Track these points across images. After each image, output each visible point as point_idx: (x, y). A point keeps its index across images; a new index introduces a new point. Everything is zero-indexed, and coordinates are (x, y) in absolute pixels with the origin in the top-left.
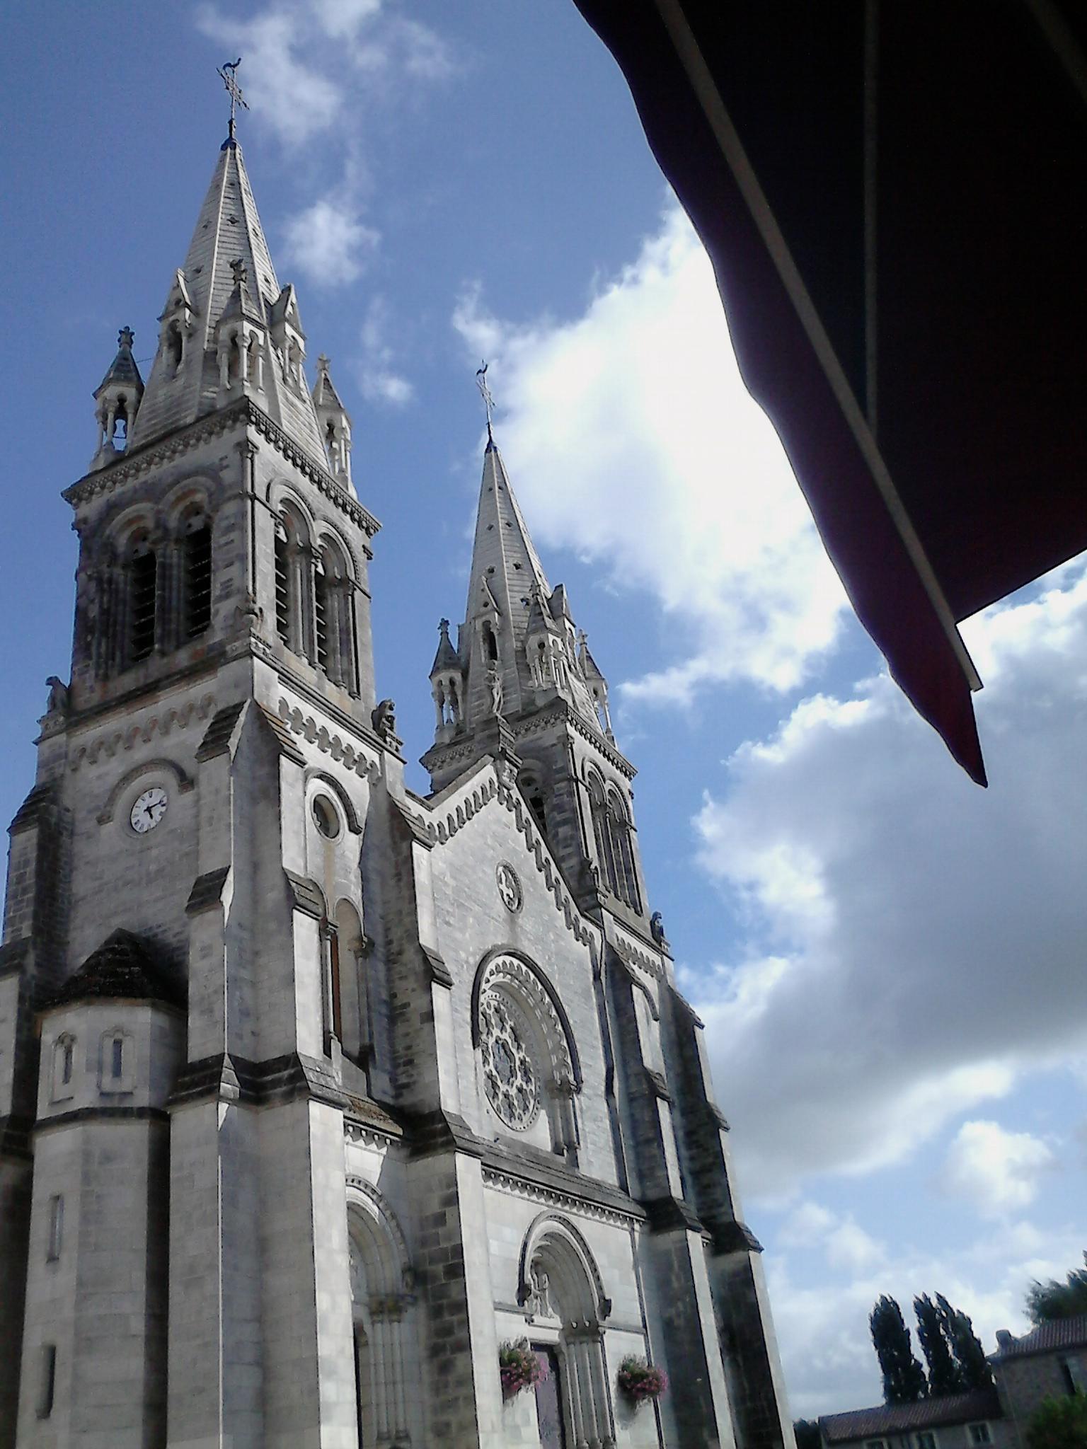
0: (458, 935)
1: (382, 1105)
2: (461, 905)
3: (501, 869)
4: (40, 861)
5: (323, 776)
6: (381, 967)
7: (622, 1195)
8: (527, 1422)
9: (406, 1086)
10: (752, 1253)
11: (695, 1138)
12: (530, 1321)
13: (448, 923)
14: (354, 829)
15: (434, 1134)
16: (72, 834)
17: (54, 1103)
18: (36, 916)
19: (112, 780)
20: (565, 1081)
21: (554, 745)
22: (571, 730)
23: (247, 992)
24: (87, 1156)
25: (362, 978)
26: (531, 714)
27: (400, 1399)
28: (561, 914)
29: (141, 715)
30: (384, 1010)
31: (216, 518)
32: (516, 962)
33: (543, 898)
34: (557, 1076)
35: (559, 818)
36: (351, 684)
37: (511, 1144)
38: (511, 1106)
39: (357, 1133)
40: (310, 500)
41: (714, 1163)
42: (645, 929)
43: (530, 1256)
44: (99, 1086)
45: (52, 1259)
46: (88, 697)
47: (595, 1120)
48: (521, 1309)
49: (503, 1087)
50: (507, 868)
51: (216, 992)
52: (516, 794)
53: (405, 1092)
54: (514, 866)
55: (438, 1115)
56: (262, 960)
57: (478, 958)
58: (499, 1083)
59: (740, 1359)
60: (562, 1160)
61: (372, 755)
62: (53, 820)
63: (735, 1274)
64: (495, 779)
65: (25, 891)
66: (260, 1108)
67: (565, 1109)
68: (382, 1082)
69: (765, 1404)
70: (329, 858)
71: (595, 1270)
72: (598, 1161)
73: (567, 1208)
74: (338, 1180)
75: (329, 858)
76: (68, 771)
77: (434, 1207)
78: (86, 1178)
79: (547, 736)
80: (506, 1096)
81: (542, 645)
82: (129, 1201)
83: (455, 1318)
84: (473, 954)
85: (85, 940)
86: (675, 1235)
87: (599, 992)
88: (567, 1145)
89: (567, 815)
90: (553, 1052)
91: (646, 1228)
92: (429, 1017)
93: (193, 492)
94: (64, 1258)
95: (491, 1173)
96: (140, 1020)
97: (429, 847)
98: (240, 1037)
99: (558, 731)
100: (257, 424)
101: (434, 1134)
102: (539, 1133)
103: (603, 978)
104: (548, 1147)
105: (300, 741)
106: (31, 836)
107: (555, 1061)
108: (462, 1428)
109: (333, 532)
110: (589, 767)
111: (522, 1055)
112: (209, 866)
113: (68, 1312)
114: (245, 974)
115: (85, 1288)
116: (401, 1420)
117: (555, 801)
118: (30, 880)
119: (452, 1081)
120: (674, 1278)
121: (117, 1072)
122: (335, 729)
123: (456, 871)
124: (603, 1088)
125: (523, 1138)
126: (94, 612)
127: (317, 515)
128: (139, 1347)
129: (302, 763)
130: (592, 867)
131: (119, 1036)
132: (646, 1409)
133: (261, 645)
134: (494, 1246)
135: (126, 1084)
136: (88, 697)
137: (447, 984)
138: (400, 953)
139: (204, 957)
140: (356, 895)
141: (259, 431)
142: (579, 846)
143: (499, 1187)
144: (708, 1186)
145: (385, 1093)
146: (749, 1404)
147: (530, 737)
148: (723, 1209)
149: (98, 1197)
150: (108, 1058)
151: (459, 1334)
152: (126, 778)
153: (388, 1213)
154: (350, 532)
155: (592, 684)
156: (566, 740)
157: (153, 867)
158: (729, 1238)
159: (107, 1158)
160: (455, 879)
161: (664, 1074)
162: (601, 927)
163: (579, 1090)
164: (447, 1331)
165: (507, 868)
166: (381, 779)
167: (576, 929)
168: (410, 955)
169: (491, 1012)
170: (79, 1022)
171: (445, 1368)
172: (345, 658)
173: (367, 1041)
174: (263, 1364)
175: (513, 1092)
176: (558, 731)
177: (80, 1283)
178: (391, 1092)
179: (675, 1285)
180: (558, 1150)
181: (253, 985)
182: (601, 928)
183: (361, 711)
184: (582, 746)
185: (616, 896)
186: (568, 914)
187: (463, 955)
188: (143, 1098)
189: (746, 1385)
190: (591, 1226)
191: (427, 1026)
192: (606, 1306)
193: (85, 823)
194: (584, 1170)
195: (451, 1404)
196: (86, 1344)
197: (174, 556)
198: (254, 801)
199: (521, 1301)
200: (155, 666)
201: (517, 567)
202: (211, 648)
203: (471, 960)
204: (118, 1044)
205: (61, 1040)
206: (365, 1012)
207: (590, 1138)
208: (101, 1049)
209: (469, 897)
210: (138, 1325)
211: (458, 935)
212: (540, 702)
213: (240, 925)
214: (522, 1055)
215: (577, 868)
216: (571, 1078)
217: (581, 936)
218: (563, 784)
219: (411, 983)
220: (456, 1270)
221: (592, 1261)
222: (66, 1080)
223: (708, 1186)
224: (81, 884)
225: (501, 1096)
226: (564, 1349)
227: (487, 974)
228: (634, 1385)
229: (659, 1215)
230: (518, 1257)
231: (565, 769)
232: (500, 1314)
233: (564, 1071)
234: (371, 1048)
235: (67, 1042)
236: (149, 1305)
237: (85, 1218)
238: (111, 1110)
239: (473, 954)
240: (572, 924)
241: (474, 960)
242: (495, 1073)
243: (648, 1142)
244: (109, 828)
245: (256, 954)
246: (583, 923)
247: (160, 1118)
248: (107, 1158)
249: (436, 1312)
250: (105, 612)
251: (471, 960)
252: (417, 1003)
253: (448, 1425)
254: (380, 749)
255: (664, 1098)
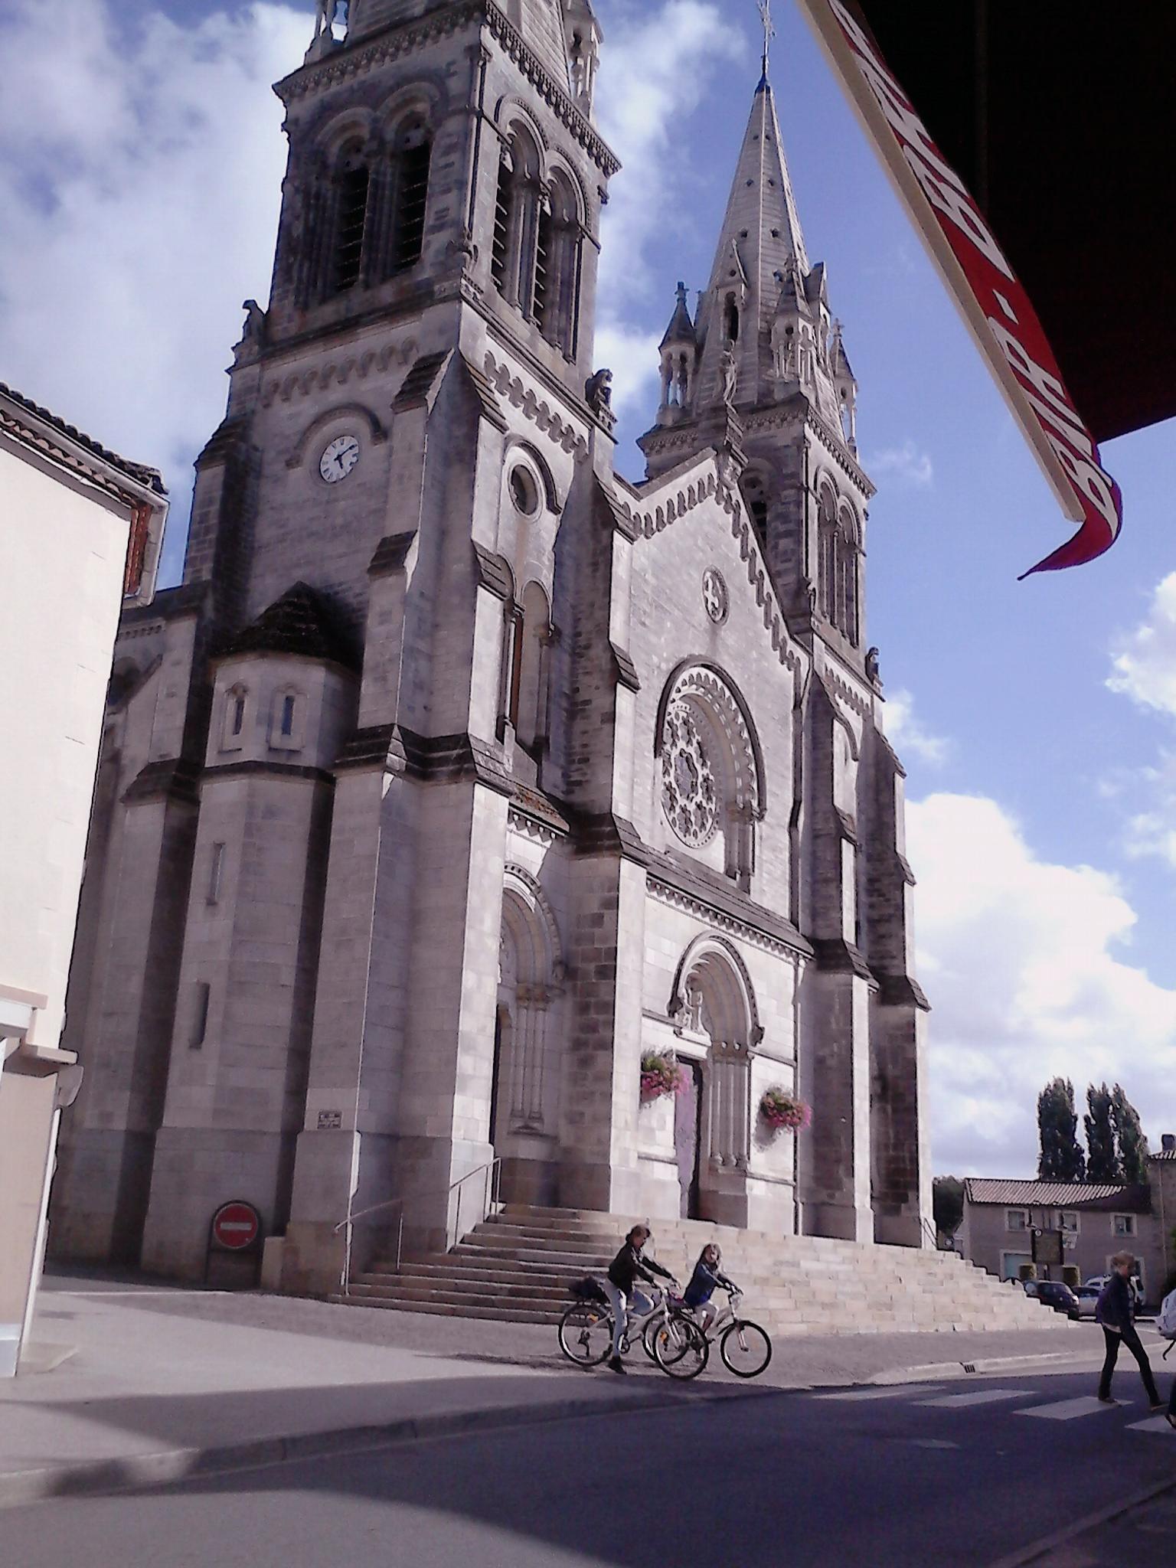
0: (653, 639)
1: (550, 798)
2: (659, 607)
3: (708, 574)
4: (224, 501)
5: (527, 446)
6: (566, 658)
7: (792, 929)
8: (663, 1128)
9: (579, 783)
10: (918, 1011)
11: (877, 885)
12: (678, 1033)
13: (643, 624)
14: (553, 508)
15: (601, 836)
16: (259, 475)
17: (221, 752)
18: (217, 560)
19: (304, 421)
20: (748, 805)
21: (787, 447)
22: (491, 43)
23: (423, 664)
24: (251, 810)
25: (544, 667)
26: (767, 408)
27: (537, 1083)
28: (769, 633)
29: (338, 352)
30: (564, 704)
31: (438, 134)
32: (712, 676)
33: (751, 613)
34: (740, 798)
35: (782, 528)
36: (567, 344)
37: (682, 858)
38: (688, 821)
39: (522, 823)
40: (544, 125)
41: (891, 916)
42: (859, 663)
43: (687, 970)
44: (268, 741)
45: (211, 903)
46: (286, 328)
47: (774, 850)
48: (670, 1020)
49: (682, 801)
50: (716, 574)
51: (390, 660)
52: (736, 495)
53: (577, 789)
54: (724, 574)
55: (609, 818)
56: (443, 633)
57: (672, 666)
58: (678, 795)
59: (889, 1108)
60: (733, 883)
61: (581, 429)
62: (242, 458)
63: (898, 1028)
64: (715, 476)
65: (207, 531)
66: (427, 783)
67: (743, 833)
68: (553, 775)
69: (907, 1155)
70: (522, 534)
71: (752, 997)
72: (772, 889)
73: (731, 931)
74: (496, 865)
75: (522, 534)
76: (260, 407)
77: (594, 908)
78: (249, 830)
79: (781, 436)
80: (684, 810)
81: (790, 331)
82: (288, 856)
83: (601, 1017)
84: (667, 661)
85: (265, 589)
86: (840, 977)
87: (797, 721)
88: (741, 869)
89: (792, 526)
90: (739, 774)
91: (812, 965)
92: (611, 718)
93: (413, 100)
94: (222, 904)
95: (656, 883)
96: (312, 679)
97: (631, 540)
98: (411, 709)
99: (794, 431)
100: (493, 26)
101: (601, 836)
102: (713, 852)
103: (804, 707)
104: (720, 867)
105: (503, 401)
106: (217, 471)
107: (740, 782)
108: (595, 1119)
109: (566, 168)
110: (823, 477)
111: (706, 771)
112: (396, 527)
113: (223, 955)
114: (422, 645)
115: (241, 936)
116: (536, 1101)
117: (781, 509)
118: (213, 521)
119: (627, 786)
120: (833, 1020)
121: (286, 729)
122: (544, 395)
123: (659, 569)
124: (787, 820)
125: (696, 855)
126: (298, 229)
127: (551, 144)
128: (288, 996)
129: (502, 428)
130: (810, 587)
131: (291, 693)
132: (785, 1138)
133: (472, 290)
134: (650, 955)
135: (294, 742)
136: (286, 328)
137: (634, 688)
138: (588, 647)
139: (381, 623)
140: (547, 579)
141: (494, 34)
142: (800, 562)
143: (664, 898)
144: (883, 937)
145: (555, 786)
146: (891, 1152)
147: (763, 433)
148: (896, 962)
149: (259, 849)
150: (279, 714)
151: (603, 1032)
152: (319, 420)
153: (545, 905)
154: (586, 169)
155: (842, 384)
156: (477, 54)
157: (339, 521)
158: (896, 990)
159: (270, 813)
160: (657, 578)
161: (855, 815)
162: (810, 654)
163: (761, 818)
164: (593, 1028)
165: (716, 574)
166: (588, 457)
167: (783, 649)
168: (597, 651)
169: (678, 723)
170: (251, 675)
171: (585, 1062)
172: (564, 316)
173: (543, 732)
174: (404, 1027)
175: (692, 807)
176: (794, 431)
177: (236, 929)
178: (564, 788)
179: (834, 1026)
180: (730, 873)
181: (430, 658)
182: (810, 654)
183: (573, 378)
184: (819, 453)
185: (832, 623)
186: (775, 634)
187: (655, 659)
188: (310, 758)
189: (892, 1135)
190: (754, 954)
191: (607, 727)
192: (759, 1034)
193: (273, 465)
194: (754, 897)
195: (588, 1096)
196: (238, 986)
197: (387, 172)
198: (447, 462)
199: (672, 1013)
200: (358, 299)
201: (775, 234)
202: (419, 285)
203: (664, 666)
204: (289, 701)
205: (233, 690)
206: (544, 702)
207: (766, 866)
208: (272, 702)
209: (670, 599)
210: (288, 976)
211: (653, 639)
212: (779, 395)
213: (422, 594)
214: (706, 771)
215: (793, 586)
216: (755, 803)
217: (787, 659)
218: (792, 492)
219: (596, 680)
220: (609, 972)
221: (750, 988)
222: (236, 731)
223: (883, 937)
224: (265, 531)
225: (678, 810)
226: (710, 1065)
227: (678, 684)
228: (775, 1112)
229: (826, 954)
230: (674, 971)
231: (795, 475)
232: (644, 1020)
233: (748, 796)
234: (547, 739)
235: (238, 692)
236: (300, 959)
237: (245, 868)
238: (277, 766)
239: (667, 661)
240: (778, 644)
241: (667, 667)
242: (674, 785)
243: (827, 881)
244: (298, 473)
245: (436, 626)
246: (791, 646)
247: (325, 780)
248: (270, 813)
249: (583, 1009)
250: (309, 231)
251: (664, 666)
252: (600, 702)
253: (582, 1114)
254: (592, 424)
255: (850, 840)
